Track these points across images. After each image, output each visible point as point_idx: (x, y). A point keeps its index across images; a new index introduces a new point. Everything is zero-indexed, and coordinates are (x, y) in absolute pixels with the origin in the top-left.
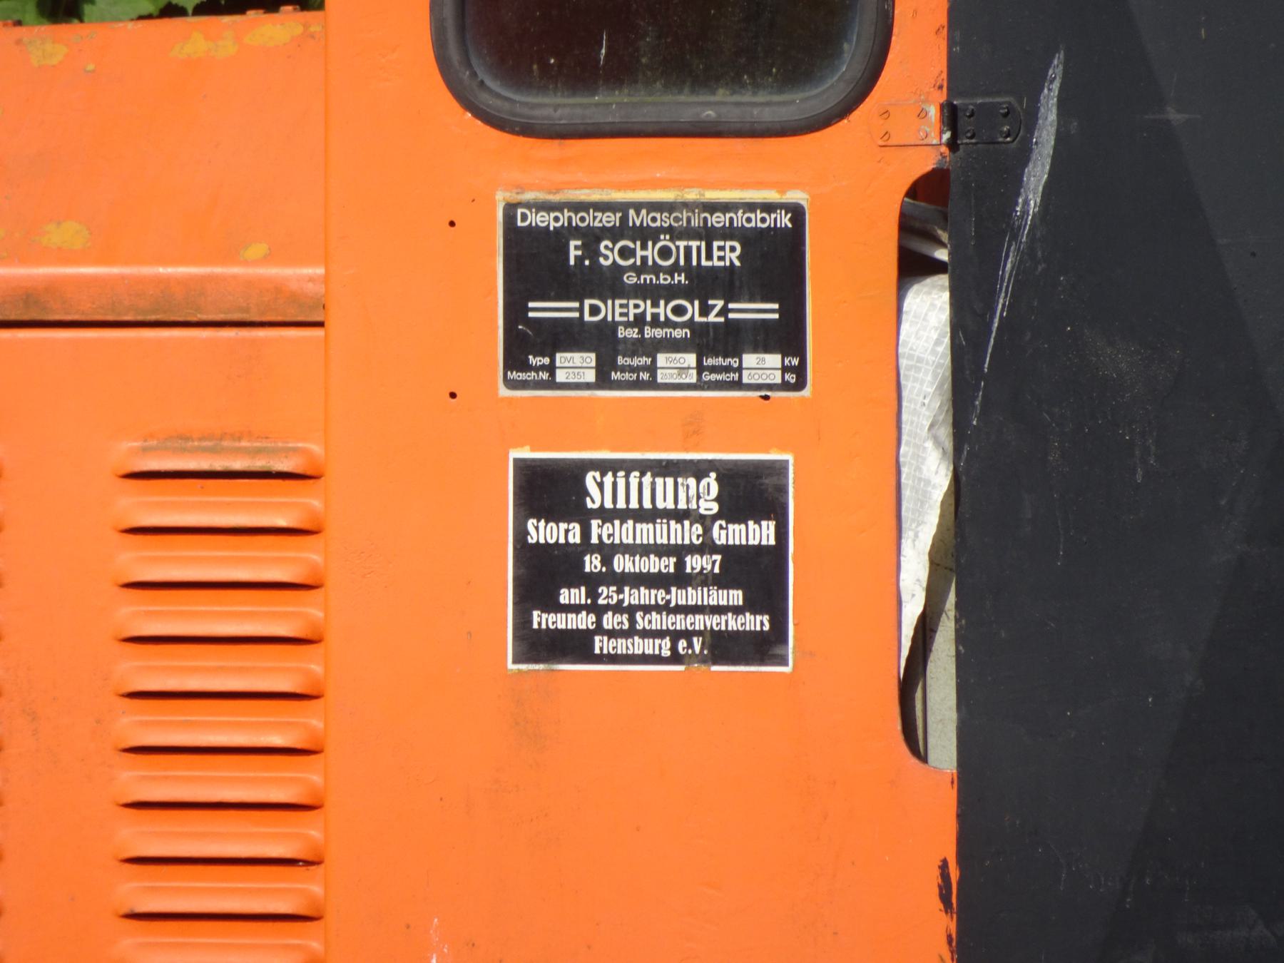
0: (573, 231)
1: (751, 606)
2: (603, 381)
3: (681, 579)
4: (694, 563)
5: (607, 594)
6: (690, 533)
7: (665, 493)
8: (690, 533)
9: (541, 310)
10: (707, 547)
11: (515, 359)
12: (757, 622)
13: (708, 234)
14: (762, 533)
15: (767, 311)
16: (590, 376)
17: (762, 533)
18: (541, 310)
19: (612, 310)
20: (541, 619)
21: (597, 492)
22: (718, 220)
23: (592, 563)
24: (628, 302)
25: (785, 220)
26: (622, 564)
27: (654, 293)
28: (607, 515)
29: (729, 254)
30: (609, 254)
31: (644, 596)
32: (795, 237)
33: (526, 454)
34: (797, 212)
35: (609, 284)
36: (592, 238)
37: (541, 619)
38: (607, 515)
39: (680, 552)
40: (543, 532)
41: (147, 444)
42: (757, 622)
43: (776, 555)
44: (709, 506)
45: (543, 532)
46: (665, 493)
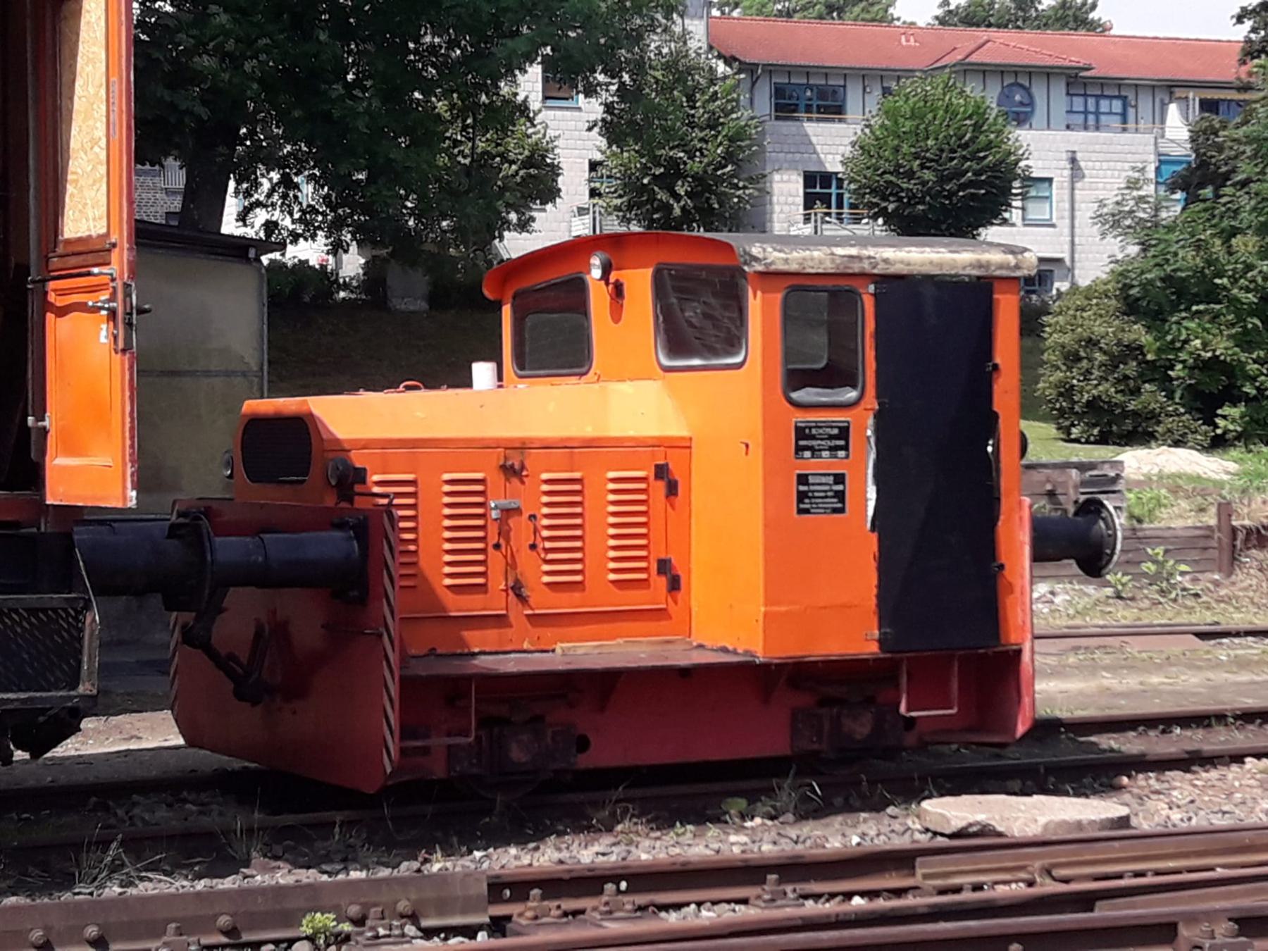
0: (806, 427)
1: (840, 502)
2: (813, 457)
3: (826, 497)
4: (830, 494)
5: (813, 500)
6: (827, 488)
7: (824, 480)
8: (827, 488)
9: (802, 443)
10: (831, 490)
11: (796, 453)
12: (839, 505)
13: (832, 427)
14: (840, 487)
15: (842, 443)
16: (810, 477)
17: (840, 487)
18: (802, 443)
19: (814, 443)
20: (802, 506)
21: (811, 480)
22: (834, 424)
23: (810, 494)
24: (770, 277)
25: (846, 424)
26: (816, 494)
27: (822, 439)
28: (813, 484)
29: (836, 431)
30: (814, 431)
31: (820, 500)
32: (848, 428)
33: (798, 472)
34: (848, 422)
35: (813, 437)
36: (810, 428)
37: (802, 506)
38: (813, 484)
39: (825, 491)
40: (802, 488)
41: (132, 891)
42: (839, 505)
43: (843, 492)
44: (831, 482)
45: (802, 488)
46: (824, 480)
